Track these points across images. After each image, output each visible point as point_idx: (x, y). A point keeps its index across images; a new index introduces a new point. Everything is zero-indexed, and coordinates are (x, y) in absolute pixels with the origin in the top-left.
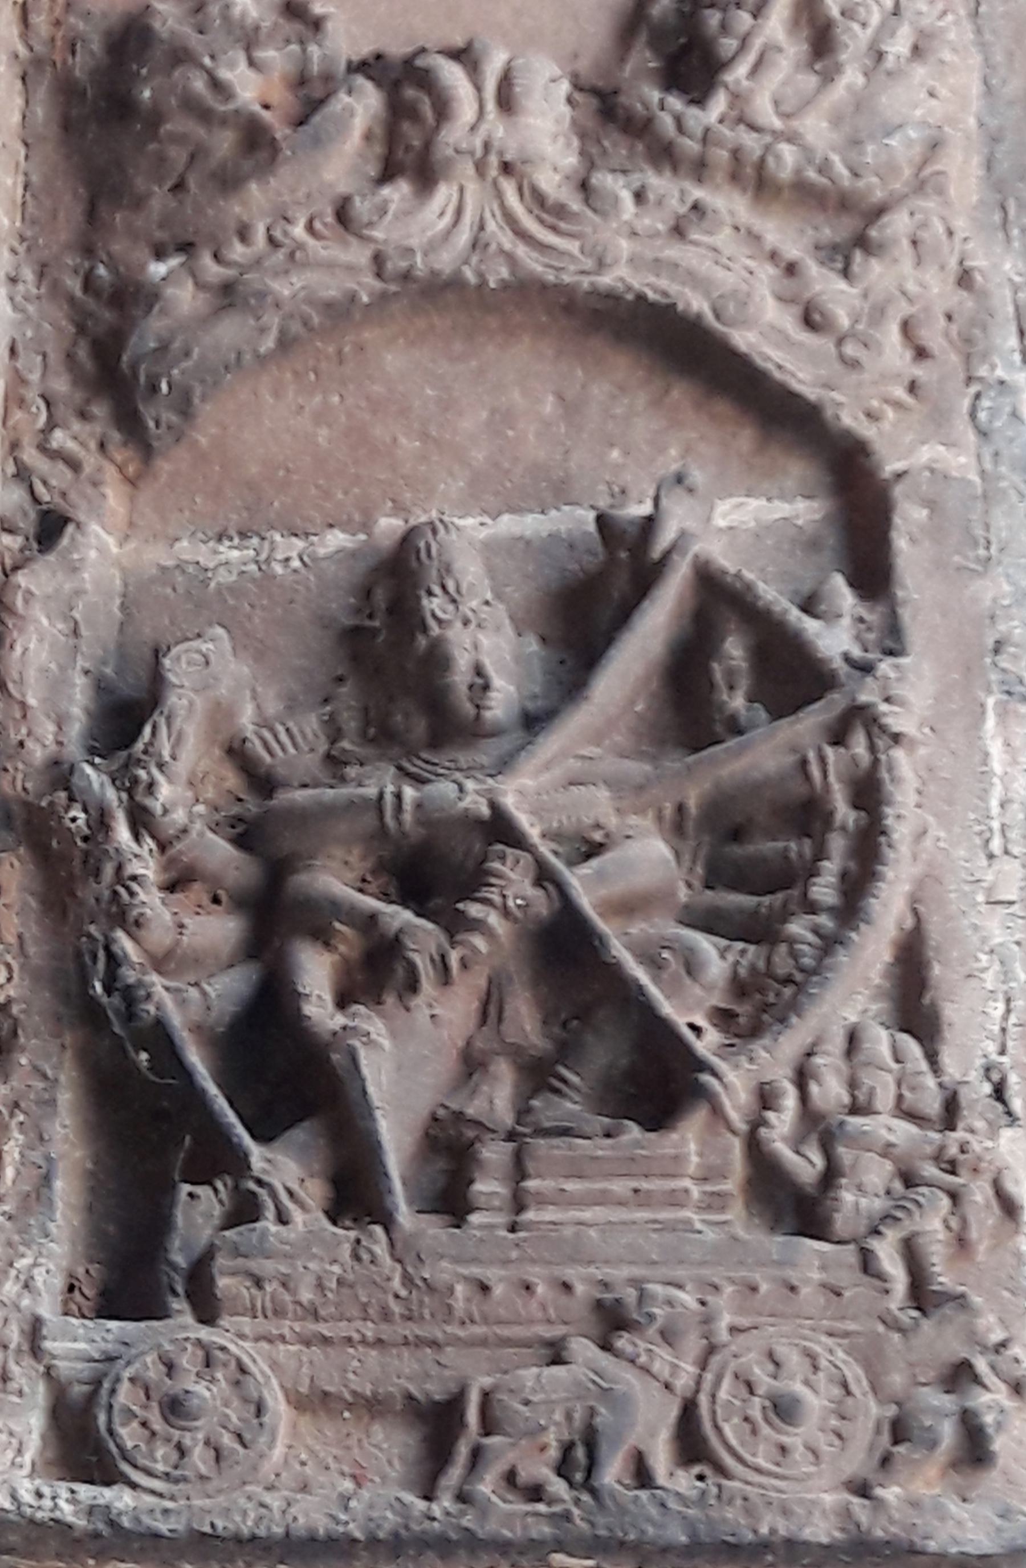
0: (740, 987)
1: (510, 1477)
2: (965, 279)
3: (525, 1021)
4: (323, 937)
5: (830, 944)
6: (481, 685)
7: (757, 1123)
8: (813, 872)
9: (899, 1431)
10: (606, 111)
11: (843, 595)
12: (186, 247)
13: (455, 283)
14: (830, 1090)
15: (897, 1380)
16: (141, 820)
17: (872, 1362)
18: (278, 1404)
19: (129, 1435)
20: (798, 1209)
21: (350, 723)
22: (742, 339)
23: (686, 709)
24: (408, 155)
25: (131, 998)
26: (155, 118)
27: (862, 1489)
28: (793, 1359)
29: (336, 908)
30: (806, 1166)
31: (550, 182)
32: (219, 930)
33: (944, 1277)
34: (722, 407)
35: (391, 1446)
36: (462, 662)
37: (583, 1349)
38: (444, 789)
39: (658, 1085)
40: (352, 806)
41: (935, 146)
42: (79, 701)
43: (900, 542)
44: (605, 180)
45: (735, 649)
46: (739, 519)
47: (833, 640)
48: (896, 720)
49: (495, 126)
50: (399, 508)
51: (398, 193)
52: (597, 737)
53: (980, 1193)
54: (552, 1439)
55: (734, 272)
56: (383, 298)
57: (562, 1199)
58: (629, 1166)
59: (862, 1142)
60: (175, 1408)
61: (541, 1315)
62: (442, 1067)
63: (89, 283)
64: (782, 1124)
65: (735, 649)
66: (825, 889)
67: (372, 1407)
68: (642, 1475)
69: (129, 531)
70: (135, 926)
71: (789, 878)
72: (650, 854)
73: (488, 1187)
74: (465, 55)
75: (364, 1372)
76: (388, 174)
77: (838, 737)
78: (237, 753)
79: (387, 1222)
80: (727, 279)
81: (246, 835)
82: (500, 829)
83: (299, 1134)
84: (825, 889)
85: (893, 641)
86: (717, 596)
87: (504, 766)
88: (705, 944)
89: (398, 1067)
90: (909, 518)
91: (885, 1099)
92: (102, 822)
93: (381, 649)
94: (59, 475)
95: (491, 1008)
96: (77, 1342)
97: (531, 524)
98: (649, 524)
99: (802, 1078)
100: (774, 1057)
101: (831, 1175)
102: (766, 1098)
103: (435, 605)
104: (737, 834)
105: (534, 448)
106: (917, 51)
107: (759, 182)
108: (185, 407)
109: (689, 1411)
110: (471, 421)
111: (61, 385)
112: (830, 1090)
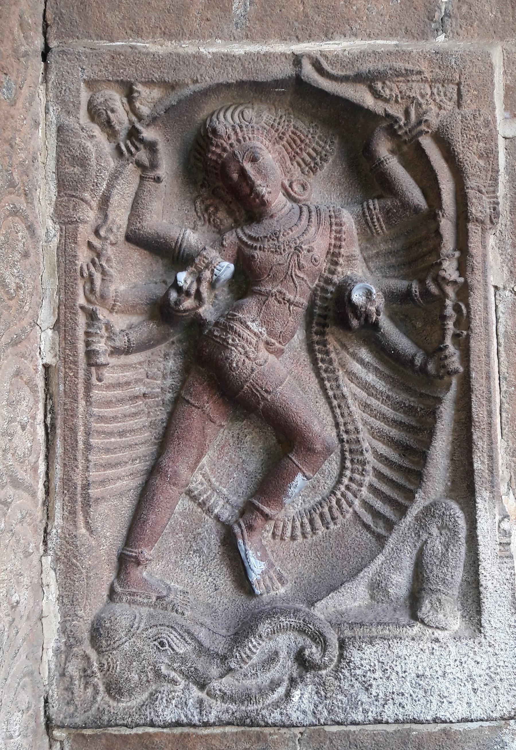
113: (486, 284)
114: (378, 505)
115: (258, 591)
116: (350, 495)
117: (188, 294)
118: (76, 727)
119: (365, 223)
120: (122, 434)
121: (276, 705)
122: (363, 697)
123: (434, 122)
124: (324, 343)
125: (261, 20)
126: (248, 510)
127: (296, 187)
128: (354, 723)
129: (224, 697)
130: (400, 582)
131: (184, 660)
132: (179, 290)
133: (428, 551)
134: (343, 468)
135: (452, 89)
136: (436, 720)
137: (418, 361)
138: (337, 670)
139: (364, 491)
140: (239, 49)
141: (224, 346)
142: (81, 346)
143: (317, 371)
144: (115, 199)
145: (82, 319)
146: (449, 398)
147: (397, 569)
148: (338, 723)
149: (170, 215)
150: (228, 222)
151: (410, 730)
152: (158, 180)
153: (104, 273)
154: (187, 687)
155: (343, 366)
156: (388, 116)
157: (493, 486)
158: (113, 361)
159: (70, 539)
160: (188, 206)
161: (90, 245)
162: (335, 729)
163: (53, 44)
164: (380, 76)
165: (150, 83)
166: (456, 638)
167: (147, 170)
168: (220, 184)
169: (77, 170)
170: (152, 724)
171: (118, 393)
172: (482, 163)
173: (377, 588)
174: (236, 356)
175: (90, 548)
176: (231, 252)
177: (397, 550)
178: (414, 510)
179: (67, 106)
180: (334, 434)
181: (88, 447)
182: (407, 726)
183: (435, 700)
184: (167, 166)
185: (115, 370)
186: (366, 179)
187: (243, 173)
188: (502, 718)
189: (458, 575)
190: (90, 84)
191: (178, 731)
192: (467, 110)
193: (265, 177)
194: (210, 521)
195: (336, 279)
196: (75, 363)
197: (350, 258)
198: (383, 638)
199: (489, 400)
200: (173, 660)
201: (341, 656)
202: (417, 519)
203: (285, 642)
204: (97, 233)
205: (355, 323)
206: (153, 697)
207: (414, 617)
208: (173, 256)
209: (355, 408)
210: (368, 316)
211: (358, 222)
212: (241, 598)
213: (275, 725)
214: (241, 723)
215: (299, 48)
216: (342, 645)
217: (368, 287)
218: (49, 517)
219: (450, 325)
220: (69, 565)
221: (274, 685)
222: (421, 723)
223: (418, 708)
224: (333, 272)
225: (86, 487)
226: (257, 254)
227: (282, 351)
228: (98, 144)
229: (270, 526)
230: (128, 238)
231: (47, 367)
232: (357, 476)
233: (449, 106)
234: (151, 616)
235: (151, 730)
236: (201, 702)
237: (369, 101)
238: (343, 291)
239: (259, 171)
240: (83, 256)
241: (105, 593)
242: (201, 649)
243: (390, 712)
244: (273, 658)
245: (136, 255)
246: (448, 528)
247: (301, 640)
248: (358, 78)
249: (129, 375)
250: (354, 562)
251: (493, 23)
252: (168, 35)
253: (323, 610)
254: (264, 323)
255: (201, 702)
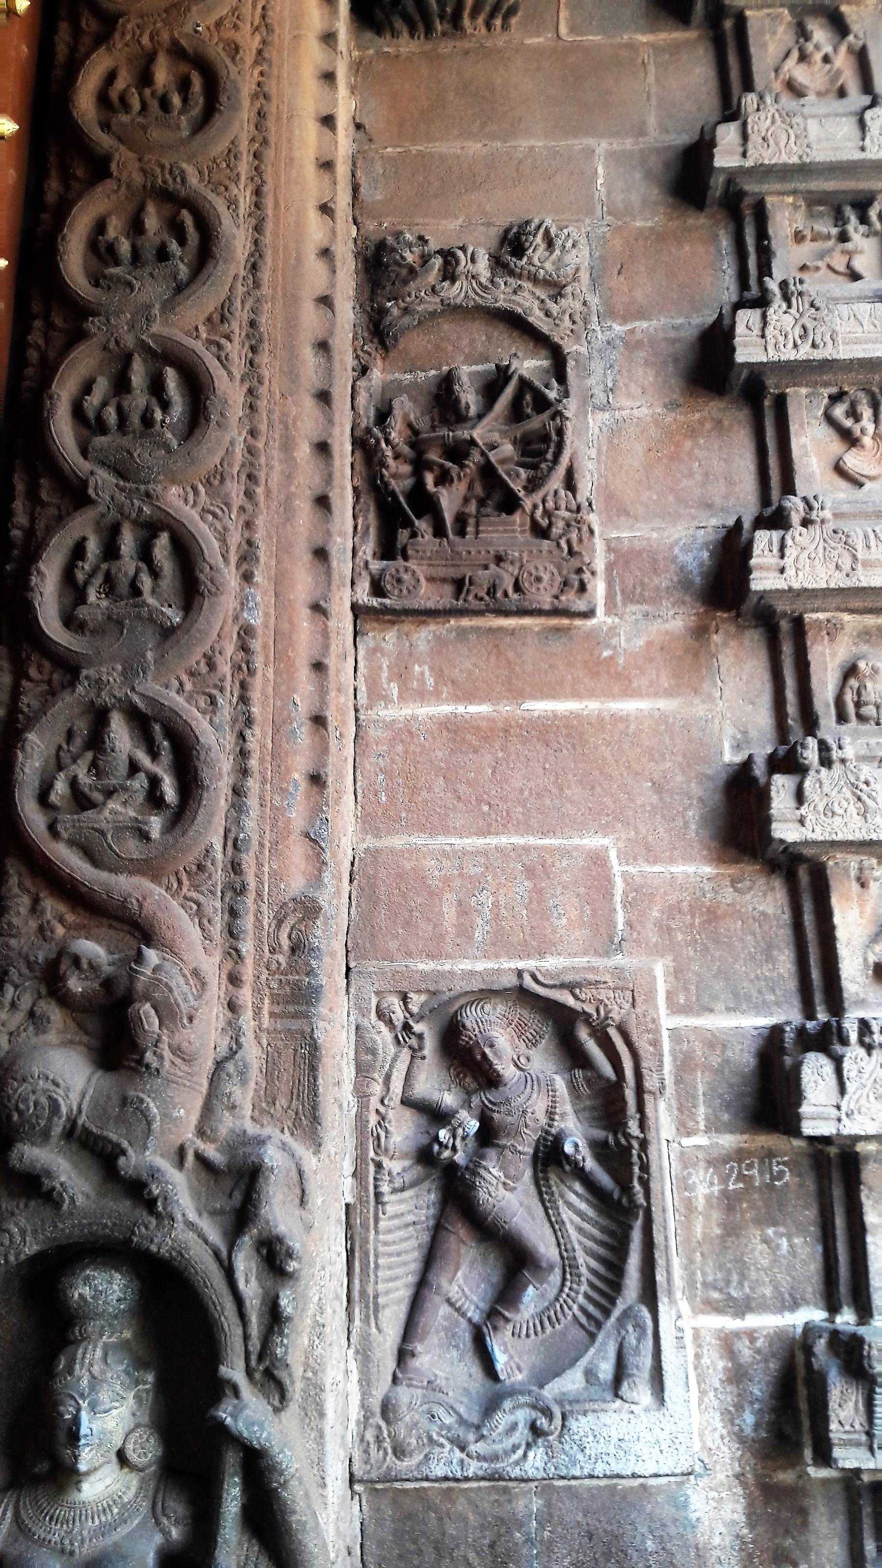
0: (530, 480)
1: (476, 596)
2: (585, 303)
3: (479, 490)
4: (431, 470)
5: (551, 469)
6: (468, 407)
7: (533, 513)
8: (547, 452)
9: (565, 583)
10: (498, 263)
11: (555, 384)
12: (395, 299)
13: (461, 306)
14: (550, 504)
15: (565, 572)
16: (388, 442)
17: (559, 568)
18: (423, 580)
19: (389, 587)
20: (541, 532)
21: (437, 417)
22: (531, 319)
23: (516, 413)
24: (449, 274)
25: (386, 484)
26: (387, 266)
27: (557, 597)
28: (541, 568)
29: (433, 463)
30: (544, 523)
31: (483, 280)
32: (406, 469)
33: (576, 548)
34: (526, 337)
35: (448, 589)
36: (463, 402)
37: (492, 566)
38: (459, 433)
39: (509, 504)
40: (438, 437)
41: (577, 270)
42: (372, 413)
43: (569, 370)
44: (497, 279)
45: (528, 397)
46: (530, 365)
47: (552, 395)
48: (567, 414)
49: (470, 266)
50: (448, 364)
51: (446, 284)
52: (496, 420)
53: (585, 528)
54: (485, 587)
55: (528, 302)
56: (443, 311)
57: (488, 532)
58: (504, 523)
59: (557, 517)
60: (399, 581)
61: (482, 558)
62: (459, 501)
63: (372, 308)
64: (539, 512)
65: (528, 397)
66: (549, 456)
67: (444, 580)
68: (506, 594)
69: (383, 371)
70: (387, 468)
71: (541, 454)
72: (508, 449)
73: (470, 529)
74: (463, 249)
75: (441, 572)
76: (444, 280)
77: (553, 418)
78: (410, 426)
79: (447, 537)
80: (527, 304)
81: (412, 445)
82: (472, 442)
83: (427, 517)
84: (549, 456)
85: (567, 394)
86: (525, 384)
87: (473, 427)
88: (522, 471)
89: (449, 501)
90: (571, 363)
91: (563, 506)
92: (378, 441)
93: (443, 399)
94: (366, 357)
95: (470, 487)
96: (376, 566)
97: (480, 368)
98: (508, 366)
99: (544, 501)
100: (537, 497)
101: (550, 525)
102: (535, 507)
103: (457, 387)
104: (529, 443)
105: (480, 348)
106: (574, 246)
107: (534, 279)
108: (396, 339)
109: (517, 581)
110: (465, 342)
111: (366, 334)
112: (550, 504)
113: (659, 1139)
114: (591, 1308)
115: (502, 1377)
116: (570, 1301)
117: (446, 1147)
118: (372, 1482)
119: (573, 1087)
120: (399, 1254)
121: (517, 1463)
122: (580, 1456)
123: (617, 1018)
124: (547, 1180)
125: (494, 944)
126: (493, 1315)
127: (523, 1060)
128: (574, 1478)
129: (480, 1458)
130: (606, 1369)
131: (449, 1429)
132: (440, 1144)
133: (626, 1345)
134: (564, 1279)
135: (628, 994)
136: (634, 1476)
137: (616, 1196)
138: (561, 1435)
139: (581, 1299)
140: (481, 966)
141: (473, 1187)
142: (371, 1188)
143: (543, 1201)
144: (393, 1078)
145: (372, 1168)
146: (638, 1224)
147: (604, 1358)
148: (563, 1478)
149: (433, 1084)
150: (474, 1085)
151: (616, 1485)
152: (423, 1058)
153: (387, 1132)
154: (451, 1450)
155: (562, 1196)
156: (584, 1012)
157: (670, 1293)
158: (393, 1197)
159: (365, 1337)
160: (444, 1072)
161: (377, 1111)
162: (561, 1483)
163: (352, 965)
164: (578, 985)
165: (419, 992)
166: (647, 1410)
167: (416, 1053)
168: (465, 1058)
169: (370, 1057)
170: (427, 1479)
171: (396, 1222)
172: (651, 1049)
173: (590, 1375)
174: (482, 1195)
175: (379, 1344)
176: (477, 1112)
177: (604, 1344)
178: (616, 1313)
179: (363, 1012)
180: (557, 1252)
181: (377, 1266)
182: (615, 1481)
183: (633, 1459)
184: (430, 1046)
185: (394, 1204)
186: (573, 1056)
187: (484, 1055)
188: (683, 1474)
189: (647, 1362)
190: (377, 993)
191: (445, 1485)
192: (638, 1010)
193: (499, 1058)
194: (463, 1323)
195: (553, 1131)
196: (368, 1202)
197: (563, 1115)
198: (594, 1411)
199: (665, 1228)
200: (441, 1428)
201: (563, 1426)
202: (618, 1319)
203: (523, 1416)
204: (382, 1102)
205: (567, 1168)
206: (427, 1457)
207: (617, 1395)
208: (437, 1116)
209: (572, 1231)
210: (576, 1163)
211: (568, 1087)
212: (489, 1383)
213: (516, 1479)
214: (491, 1478)
215: (521, 965)
216: (564, 1417)
217: (577, 1139)
218: (350, 1318)
219: (636, 1169)
220: (364, 1355)
221: (515, 1448)
222: (622, 1477)
223: (620, 1466)
224: (550, 1126)
225: (376, 1297)
226: (496, 1116)
227: (515, 1188)
228: (383, 1037)
229: (510, 1327)
230: (402, 1102)
231: (347, 1206)
232: (575, 1286)
233: (627, 1006)
234: (424, 1396)
235: (426, 1484)
236: (462, 1461)
237: (571, 1001)
238: (558, 1141)
239: (495, 1054)
240: (373, 1119)
241: (390, 1378)
242: (462, 1421)
243: (600, 1469)
244: (514, 1427)
245: (408, 1114)
246: (639, 1327)
247: (534, 1414)
248: (562, 986)
249: (403, 1208)
250: (573, 1354)
251: (656, 945)
252: (431, 956)
253: (550, 1391)
254: (502, 1168)
255: (462, 1461)
